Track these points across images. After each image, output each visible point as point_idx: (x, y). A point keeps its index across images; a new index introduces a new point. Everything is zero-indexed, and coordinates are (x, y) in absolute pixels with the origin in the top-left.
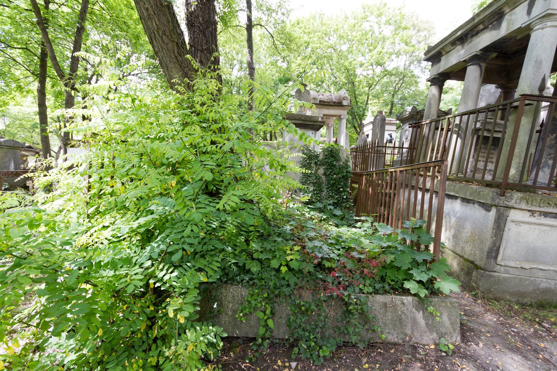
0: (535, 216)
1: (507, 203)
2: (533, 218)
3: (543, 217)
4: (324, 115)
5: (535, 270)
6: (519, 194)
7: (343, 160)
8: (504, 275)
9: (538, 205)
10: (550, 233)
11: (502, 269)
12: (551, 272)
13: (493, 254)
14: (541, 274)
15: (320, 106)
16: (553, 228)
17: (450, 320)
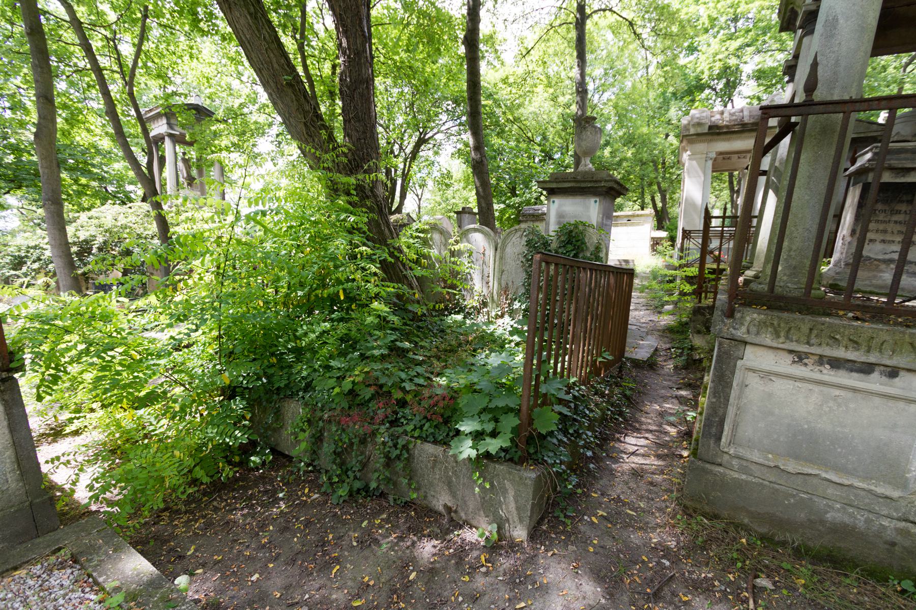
0: (806, 365)
1: (734, 332)
2: (803, 368)
3: (828, 366)
4: (721, 153)
5: (815, 481)
6: (755, 315)
7: (592, 249)
8: (736, 475)
9: (803, 339)
10: (852, 406)
11: (735, 462)
12: (862, 493)
13: (714, 430)
14: (831, 491)
15: (710, 137)
16: (859, 396)
17: (516, 502)
